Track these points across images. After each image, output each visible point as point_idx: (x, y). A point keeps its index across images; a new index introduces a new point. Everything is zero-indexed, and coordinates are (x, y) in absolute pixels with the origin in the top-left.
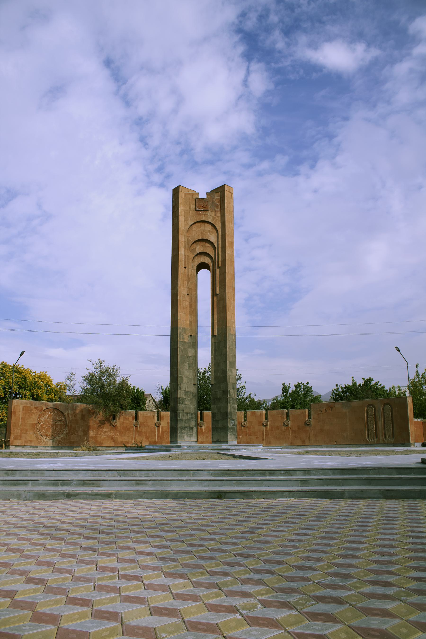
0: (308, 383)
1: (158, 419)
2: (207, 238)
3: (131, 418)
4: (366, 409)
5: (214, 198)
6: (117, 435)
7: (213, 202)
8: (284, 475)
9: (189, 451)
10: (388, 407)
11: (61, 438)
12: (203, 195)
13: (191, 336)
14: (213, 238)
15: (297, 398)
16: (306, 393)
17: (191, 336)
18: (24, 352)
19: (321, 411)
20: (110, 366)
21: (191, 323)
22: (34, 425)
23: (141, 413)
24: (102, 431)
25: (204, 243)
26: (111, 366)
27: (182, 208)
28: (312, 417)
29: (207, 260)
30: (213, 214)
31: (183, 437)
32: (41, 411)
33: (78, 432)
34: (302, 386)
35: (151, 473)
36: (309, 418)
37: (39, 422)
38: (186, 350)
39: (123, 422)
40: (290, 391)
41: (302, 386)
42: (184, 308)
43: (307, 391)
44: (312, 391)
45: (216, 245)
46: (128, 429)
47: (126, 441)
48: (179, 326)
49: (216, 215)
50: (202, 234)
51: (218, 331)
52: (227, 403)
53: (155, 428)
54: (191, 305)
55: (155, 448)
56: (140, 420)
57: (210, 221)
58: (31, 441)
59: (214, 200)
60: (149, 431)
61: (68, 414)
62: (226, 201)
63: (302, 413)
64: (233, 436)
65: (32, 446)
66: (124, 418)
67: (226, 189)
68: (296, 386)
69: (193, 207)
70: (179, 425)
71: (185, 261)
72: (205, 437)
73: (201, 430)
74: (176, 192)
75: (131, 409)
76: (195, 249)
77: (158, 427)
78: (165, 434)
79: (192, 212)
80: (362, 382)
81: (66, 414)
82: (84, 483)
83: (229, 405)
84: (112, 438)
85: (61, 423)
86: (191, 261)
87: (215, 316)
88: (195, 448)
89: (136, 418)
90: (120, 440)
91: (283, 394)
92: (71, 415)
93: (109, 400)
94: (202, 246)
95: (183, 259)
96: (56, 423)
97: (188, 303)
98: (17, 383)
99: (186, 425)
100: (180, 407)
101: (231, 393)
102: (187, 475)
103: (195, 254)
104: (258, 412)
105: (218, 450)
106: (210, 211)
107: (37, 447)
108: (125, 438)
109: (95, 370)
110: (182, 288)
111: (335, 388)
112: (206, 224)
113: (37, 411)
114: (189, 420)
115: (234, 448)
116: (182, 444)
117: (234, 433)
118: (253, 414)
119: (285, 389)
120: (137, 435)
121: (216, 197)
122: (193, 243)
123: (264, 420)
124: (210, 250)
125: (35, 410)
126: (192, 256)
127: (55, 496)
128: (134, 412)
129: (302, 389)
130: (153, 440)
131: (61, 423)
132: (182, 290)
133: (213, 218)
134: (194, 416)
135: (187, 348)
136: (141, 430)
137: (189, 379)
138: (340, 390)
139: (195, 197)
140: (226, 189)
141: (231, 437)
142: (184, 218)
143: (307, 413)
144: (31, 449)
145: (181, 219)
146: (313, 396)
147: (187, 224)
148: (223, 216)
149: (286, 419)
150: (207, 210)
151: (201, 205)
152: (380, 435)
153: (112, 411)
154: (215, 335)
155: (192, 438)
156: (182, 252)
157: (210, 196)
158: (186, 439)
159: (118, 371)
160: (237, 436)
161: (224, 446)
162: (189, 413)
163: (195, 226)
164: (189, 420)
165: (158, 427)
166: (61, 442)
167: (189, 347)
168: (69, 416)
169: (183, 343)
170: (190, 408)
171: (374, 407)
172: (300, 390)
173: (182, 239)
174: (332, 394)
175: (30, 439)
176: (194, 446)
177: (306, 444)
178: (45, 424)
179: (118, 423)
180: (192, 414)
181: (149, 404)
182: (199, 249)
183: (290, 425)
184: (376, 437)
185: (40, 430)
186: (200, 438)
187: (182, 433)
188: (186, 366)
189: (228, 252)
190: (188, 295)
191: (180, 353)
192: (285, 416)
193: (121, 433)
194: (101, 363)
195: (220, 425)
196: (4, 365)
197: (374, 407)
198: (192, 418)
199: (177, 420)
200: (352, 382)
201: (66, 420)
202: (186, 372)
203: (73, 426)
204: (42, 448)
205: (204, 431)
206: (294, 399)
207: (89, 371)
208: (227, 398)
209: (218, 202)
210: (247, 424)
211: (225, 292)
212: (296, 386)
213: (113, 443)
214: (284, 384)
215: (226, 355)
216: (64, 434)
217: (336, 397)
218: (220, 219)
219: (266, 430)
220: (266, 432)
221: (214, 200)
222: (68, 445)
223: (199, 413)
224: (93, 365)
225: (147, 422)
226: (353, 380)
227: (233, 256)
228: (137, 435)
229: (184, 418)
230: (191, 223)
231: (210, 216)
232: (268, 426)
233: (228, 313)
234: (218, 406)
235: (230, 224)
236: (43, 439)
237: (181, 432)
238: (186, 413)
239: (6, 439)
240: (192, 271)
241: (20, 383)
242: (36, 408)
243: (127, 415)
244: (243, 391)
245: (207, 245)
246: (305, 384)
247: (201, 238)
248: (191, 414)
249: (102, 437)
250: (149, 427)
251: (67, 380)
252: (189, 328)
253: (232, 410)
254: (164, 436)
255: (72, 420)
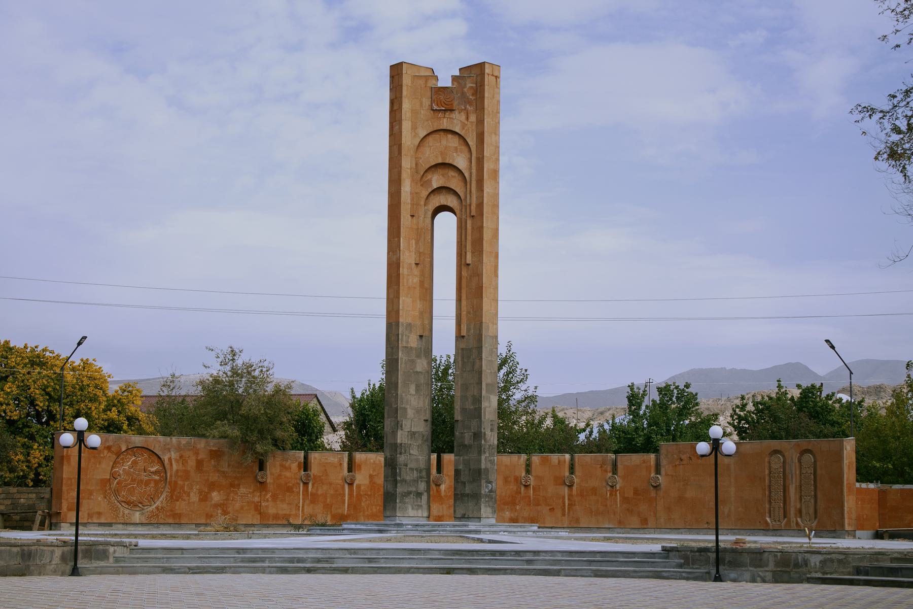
0: (687, 386)
1: (350, 469)
2: (450, 162)
3: (294, 466)
4: (767, 459)
5: (465, 86)
6: (268, 500)
7: (463, 93)
8: (514, 555)
9: (416, 533)
10: (809, 458)
11: (157, 508)
12: (445, 81)
13: (421, 336)
14: (461, 162)
15: (660, 423)
16: (684, 407)
17: (421, 336)
18: (85, 338)
19: (681, 460)
20: (252, 360)
21: (421, 313)
22: (104, 483)
23: (314, 456)
24: (237, 494)
25: (446, 171)
26: (255, 360)
27: (406, 105)
28: (663, 471)
29: (451, 201)
30: (463, 117)
31: (406, 508)
32: (119, 454)
33: (189, 495)
34: (675, 391)
35: (381, 552)
36: (658, 471)
37: (113, 476)
38: (413, 361)
39: (280, 475)
40: (647, 402)
41: (675, 391)
42: (409, 288)
43: (687, 403)
44: (697, 404)
45: (467, 175)
46: (289, 490)
47: (284, 512)
48: (401, 320)
49: (467, 119)
50: (442, 153)
51: (468, 329)
52: (480, 453)
53: (343, 487)
54: (422, 283)
55: (358, 527)
56: (315, 470)
57: (457, 130)
58: (99, 514)
59: (465, 90)
60: (332, 492)
61: (170, 459)
62: (486, 95)
63: (644, 462)
64: (489, 510)
65: (101, 524)
66: (282, 466)
67: (487, 71)
68: (660, 390)
69: (427, 102)
70: (399, 490)
71: (412, 205)
72: (445, 507)
73: (439, 491)
74: (396, 71)
75: (294, 448)
76: (430, 181)
77: (351, 484)
78: (364, 500)
79: (425, 112)
80: (796, 393)
81: (166, 458)
82: (319, 561)
83: (483, 457)
84: (257, 508)
85: (157, 478)
86: (422, 203)
87: (464, 303)
88: (425, 529)
89: (306, 466)
90: (272, 511)
91: (630, 408)
92: (176, 460)
93: (245, 431)
94: (443, 175)
95: (409, 201)
96: (146, 478)
97: (416, 280)
98: (44, 390)
99: (410, 489)
100: (401, 459)
101: (488, 437)
102: (418, 554)
103: (430, 190)
104: (555, 457)
105: (461, 532)
106: (457, 112)
107: (110, 525)
108: (283, 508)
109: (222, 368)
110: (407, 253)
111: (738, 402)
112: (450, 136)
113: (110, 454)
114: (416, 481)
115: (487, 529)
116: (405, 521)
117: (491, 504)
118: (544, 461)
119: (634, 399)
120: (307, 502)
121: (469, 85)
122: (426, 171)
123: (567, 474)
124: (455, 183)
125: (106, 452)
126: (425, 193)
127: (297, 571)
128: (302, 454)
129: (674, 399)
130: (340, 511)
131: (157, 478)
132: (408, 257)
133: (463, 126)
134: (424, 474)
135: (414, 357)
136: (314, 491)
137: (418, 411)
138: (750, 407)
139: (431, 83)
140: (487, 70)
141: (485, 511)
142: (410, 123)
143: (653, 463)
144: (100, 528)
145: (406, 126)
146: (698, 415)
147: (416, 135)
148: (480, 122)
149: (610, 474)
150: (452, 110)
151: (443, 100)
152: (792, 511)
153: (258, 453)
154: (463, 337)
155: (420, 511)
156: (407, 187)
157: (458, 83)
158: (411, 512)
159: (271, 372)
160: (498, 510)
161: (472, 526)
162: (417, 469)
163: (430, 139)
164: (416, 481)
165: (351, 484)
166: (157, 515)
167: (418, 356)
168: (171, 464)
169: (408, 349)
170: (417, 460)
171: (784, 456)
172: (671, 399)
173: (407, 163)
174: (732, 416)
175: (97, 510)
176: (424, 525)
177: (650, 525)
178: (126, 480)
179: (269, 476)
180: (421, 471)
181: (333, 440)
182: (436, 181)
183: (618, 487)
184: (785, 517)
185: (116, 492)
186: (436, 509)
187: (405, 503)
188: (412, 389)
189: (487, 189)
190: (417, 264)
191: (401, 366)
192: (609, 468)
193: (275, 497)
194: (234, 355)
195: (468, 490)
196: (7, 348)
197: (784, 456)
198: (421, 477)
199: (396, 481)
200: (777, 390)
201: (166, 473)
202: (413, 399)
203: (180, 482)
204: (120, 526)
205: (443, 494)
206: (653, 423)
207: (208, 370)
208: (480, 446)
209: (473, 95)
210: (532, 481)
211: (481, 261)
212: (660, 390)
213: (259, 516)
214: (631, 387)
215: (480, 373)
216: (161, 499)
217: (739, 423)
218: (474, 127)
219: (570, 495)
220: (569, 499)
221: (465, 90)
222: (170, 521)
223: (434, 456)
224: (218, 357)
225: (327, 475)
226: (779, 387)
227: (496, 195)
228: (307, 502)
229: (408, 478)
230: (422, 136)
231: (456, 121)
232: (574, 488)
233: (485, 299)
234: (466, 457)
235: (493, 135)
236: (122, 509)
237: (402, 501)
238: (412, 469)
239: (50, 509)
240: (424, 221)
241: (50, 389)
242: (109, 448)
243: (287, 460)
244: (532, 406)
245: (452, 173)
246: (682, 387)
247: (440, 161)
248: (419, 470)
249: (237, 506)
250: (331, 484)
251: (164, 389)
252: (418, 323)
253: (489, 466)
254: (363, 504)
255: (177, 471)
